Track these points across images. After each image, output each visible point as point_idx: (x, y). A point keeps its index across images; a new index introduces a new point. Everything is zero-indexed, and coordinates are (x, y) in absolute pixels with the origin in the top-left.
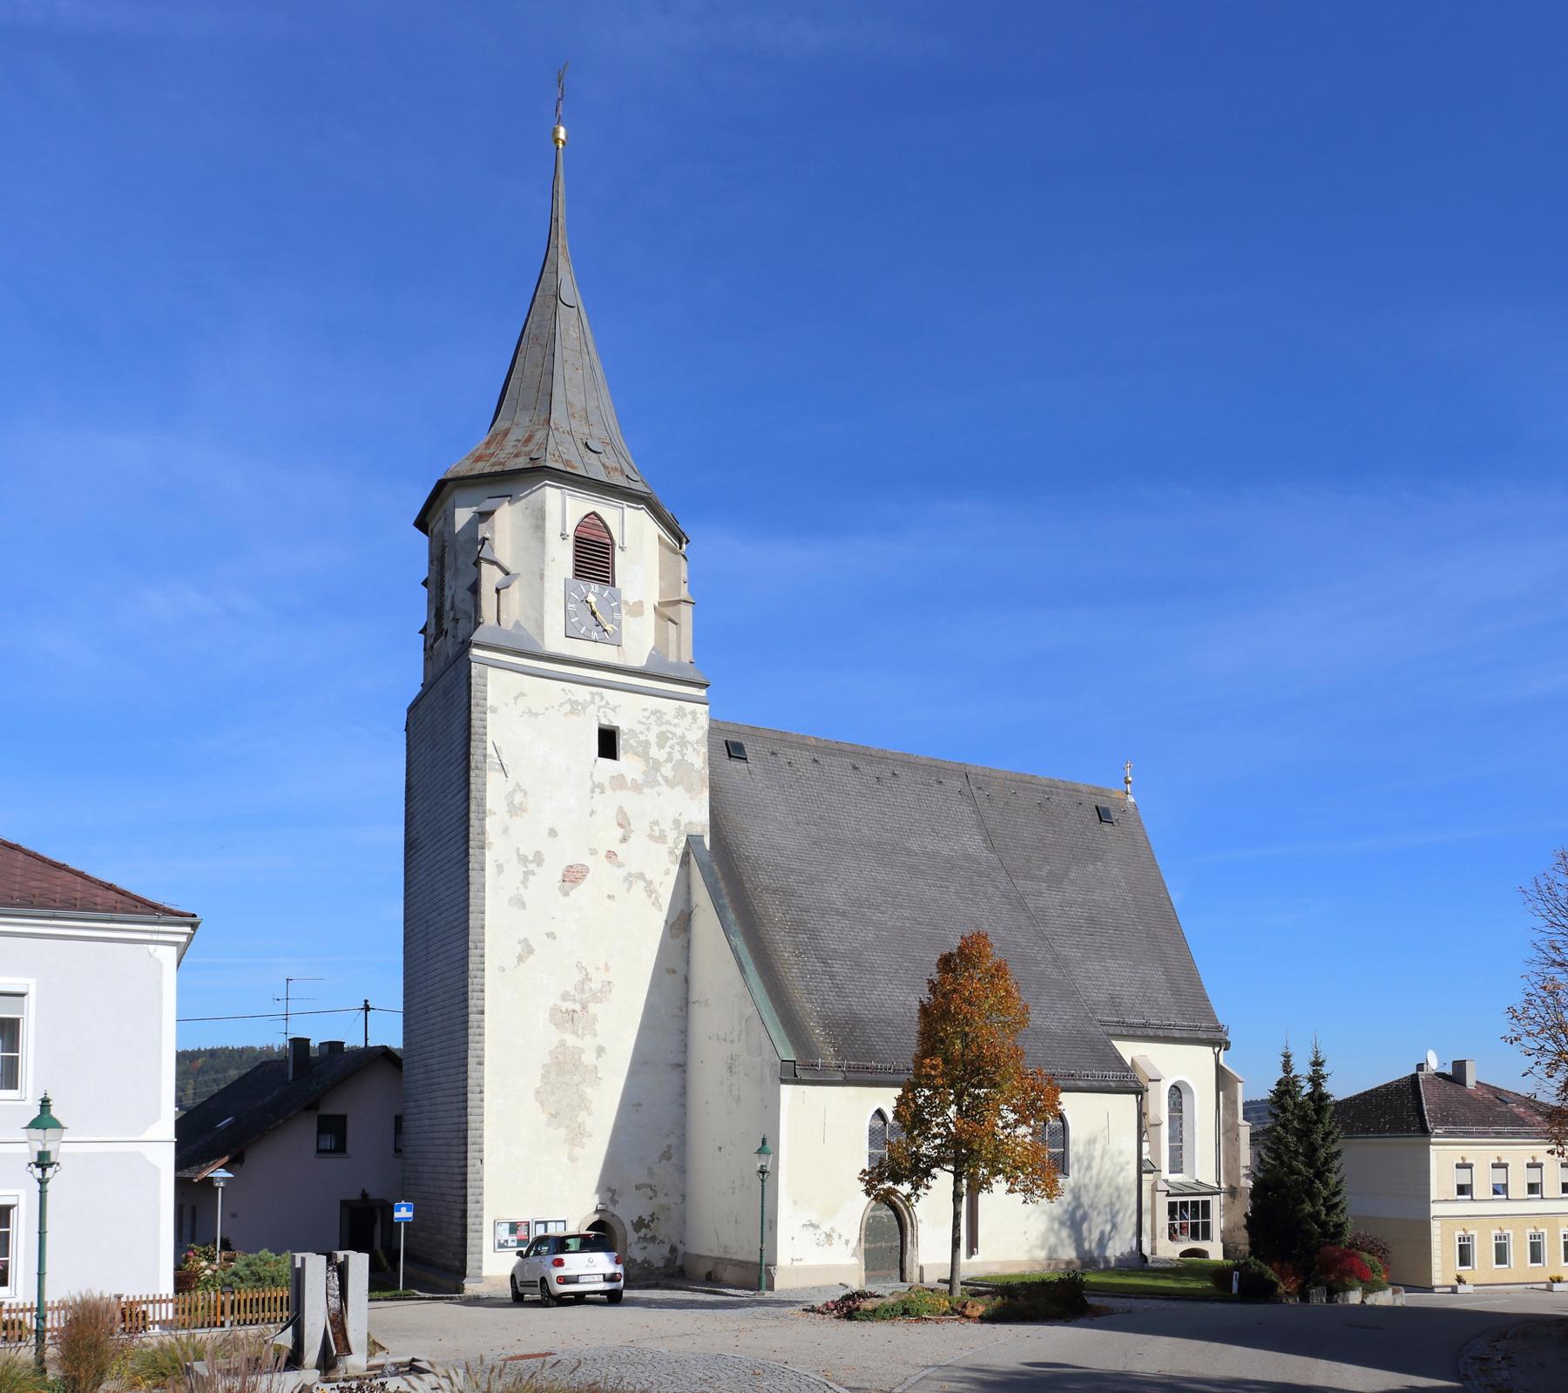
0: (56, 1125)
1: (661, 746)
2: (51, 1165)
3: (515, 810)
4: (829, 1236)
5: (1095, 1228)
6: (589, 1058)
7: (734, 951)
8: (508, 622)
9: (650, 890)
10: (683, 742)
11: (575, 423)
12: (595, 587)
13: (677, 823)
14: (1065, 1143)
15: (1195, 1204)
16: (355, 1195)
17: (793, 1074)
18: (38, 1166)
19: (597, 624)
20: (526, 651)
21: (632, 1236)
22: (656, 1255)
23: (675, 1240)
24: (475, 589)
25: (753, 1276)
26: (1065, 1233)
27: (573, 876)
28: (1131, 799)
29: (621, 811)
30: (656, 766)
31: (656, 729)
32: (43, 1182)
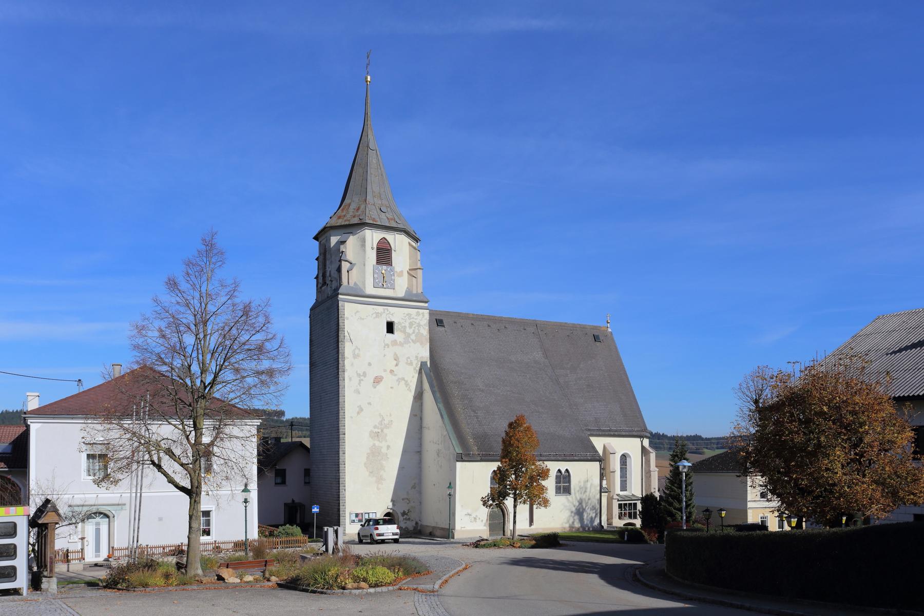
0: (249, 491)
1: (410, 327)
3: (356, 356)
4: (475, 519)
5: (589, 514)
6: (384, 450)
7: (439, 409)
8: (352, 284)
9: (407, 384)
10: (419, 325)
11: (376, 200)
12: (385, 267)
13: (417, 357)
14: (569, 482)
15: (630, 504)
16: (290, 501)
17: (461, 458)
19: (384, 281)
20: (359, 294)
21: (401, 518)
22: (410, 525)
23: (417, 520)
24: (339, 270)
25: (446, 534)
26: (576, 517)
27: (378, 380)
28: (610, 330)
29: (395, 354)
30: (409, 335)
31: (408, 321)
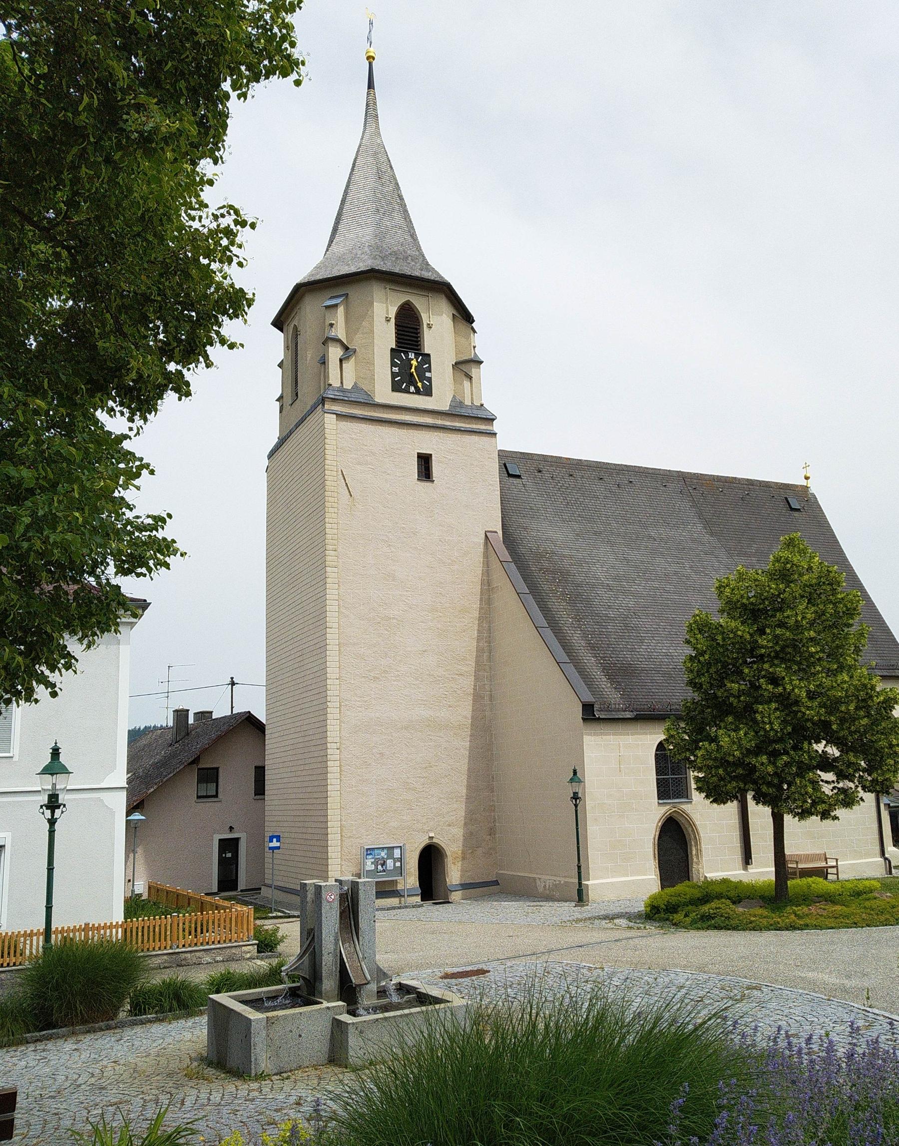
0: (64, 770)
2: (58, 807)
18: (48, 807)
32: (52, 822)
